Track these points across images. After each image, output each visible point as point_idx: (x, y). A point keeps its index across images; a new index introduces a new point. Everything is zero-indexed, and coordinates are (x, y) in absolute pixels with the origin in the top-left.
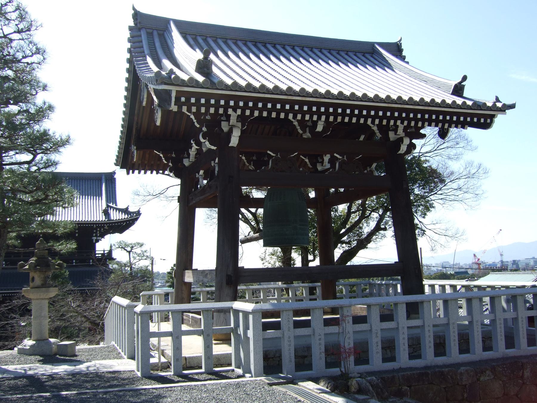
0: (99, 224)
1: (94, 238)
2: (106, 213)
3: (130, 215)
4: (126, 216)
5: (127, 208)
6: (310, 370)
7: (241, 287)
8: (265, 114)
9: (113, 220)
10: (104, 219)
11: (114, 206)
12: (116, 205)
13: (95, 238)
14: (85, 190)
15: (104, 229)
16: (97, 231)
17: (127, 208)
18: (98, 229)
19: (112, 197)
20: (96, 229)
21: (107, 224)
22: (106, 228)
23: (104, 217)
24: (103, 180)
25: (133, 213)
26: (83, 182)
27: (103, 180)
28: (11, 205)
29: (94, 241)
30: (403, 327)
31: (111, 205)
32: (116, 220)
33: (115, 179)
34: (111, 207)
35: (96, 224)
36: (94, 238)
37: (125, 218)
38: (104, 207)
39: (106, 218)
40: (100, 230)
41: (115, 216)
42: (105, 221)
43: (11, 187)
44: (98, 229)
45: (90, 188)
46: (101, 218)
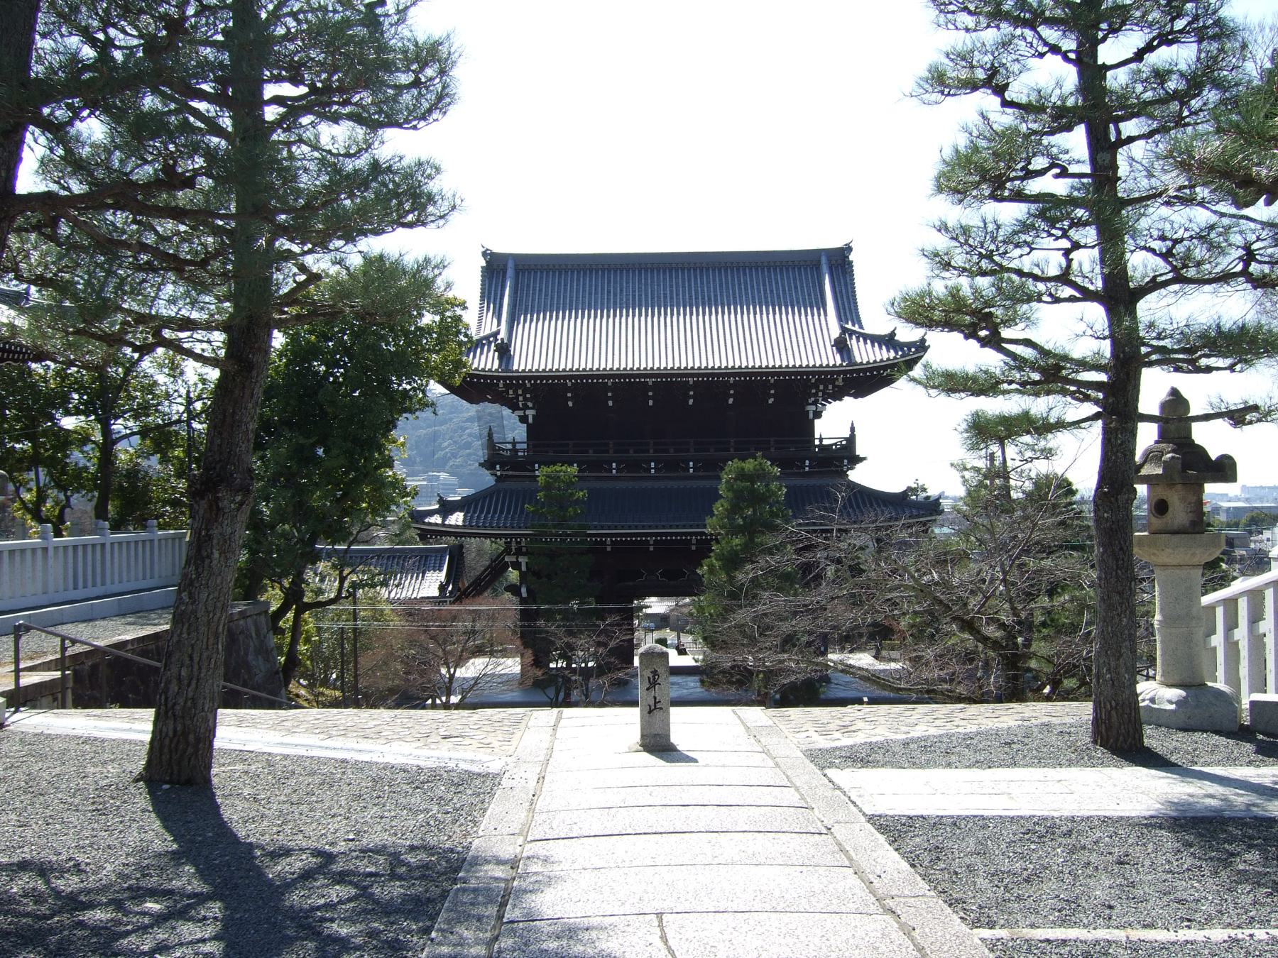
0: (820, 373)
1: (811, 408)
2: (841, 346)
3: (902, 349)
4: (892, 354)
5: (893, 334)
6: (1250, 687)
7: (324, 178)
8: (530, 404)
9: (861, 364)
10: (839, 362)
11: (856, 328)
12: (861, 327)
13: (813, 408)
14: (784, 292)
15: (834, 386)
16: (818, 390)
17: (893, 334)
18: (821, 387)
19: (848, 308)
20: (816, 386)
21: (844, 372)
22: (840, 382)
23: (838, 357)
24: (825, 268)
25: (910, 345)
26: (776, 275)
27: (825, 268)
28: (128, 351)
29: (811, 416)
30: (1048, 454)
31: (849, 326)
32: (868, 363)
33: (850, 264)
34: (852, 333)
35: (813, 373)
36: (811, 408)
37: (888, 359)
38: (836, 332)
39: (843, 360)
40: (826, 387)
41: (865, 354)
42: (841, 365)
43: (164, 28)
44: (821, 387)
45: (796, 288)
46: (832, 359)
